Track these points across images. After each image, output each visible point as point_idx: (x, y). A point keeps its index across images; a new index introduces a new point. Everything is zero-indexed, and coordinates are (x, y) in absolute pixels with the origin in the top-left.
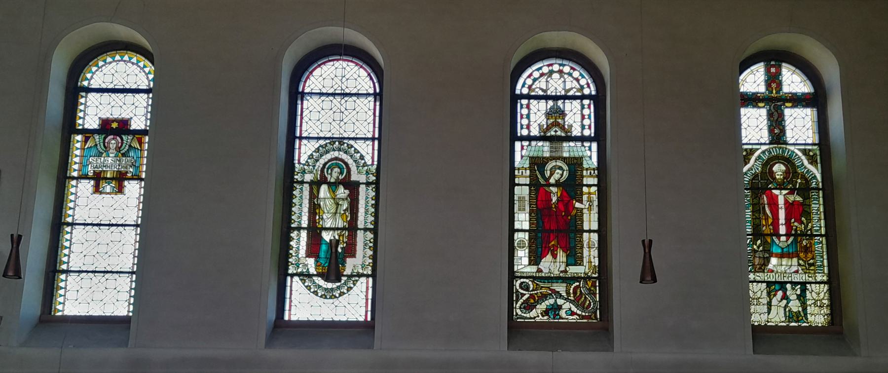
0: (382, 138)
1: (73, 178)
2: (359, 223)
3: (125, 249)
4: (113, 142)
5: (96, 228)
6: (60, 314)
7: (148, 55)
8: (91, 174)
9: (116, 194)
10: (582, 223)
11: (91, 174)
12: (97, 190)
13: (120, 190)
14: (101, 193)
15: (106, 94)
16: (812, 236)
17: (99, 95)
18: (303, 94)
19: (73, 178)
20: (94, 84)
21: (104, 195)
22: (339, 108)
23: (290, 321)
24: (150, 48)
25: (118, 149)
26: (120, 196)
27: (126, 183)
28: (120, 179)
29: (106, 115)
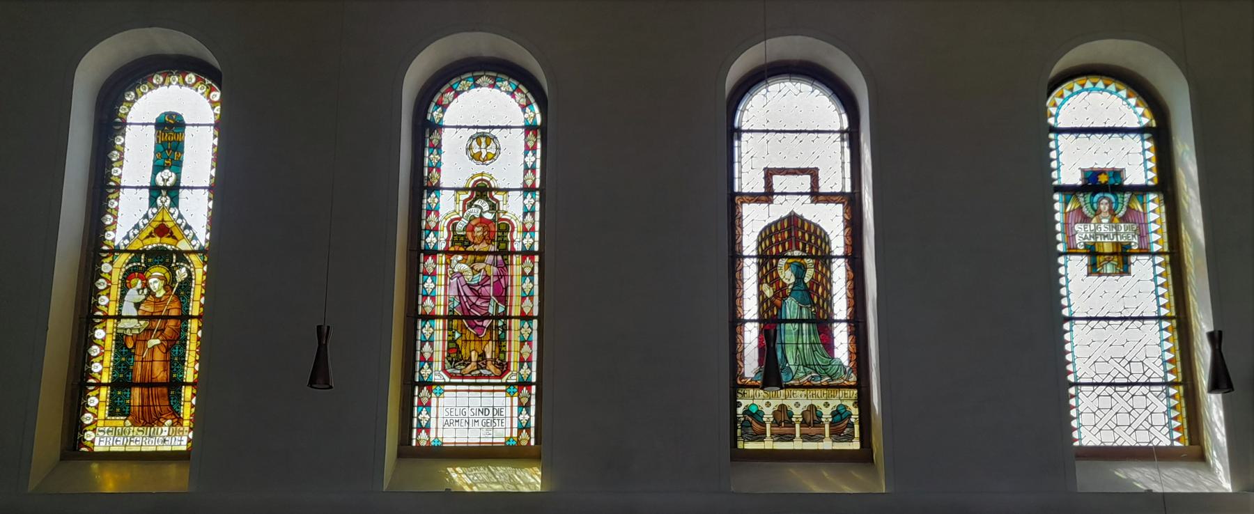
0: (552, 189)
1: (1061, 254)
2: (836, 310)
3: (1085, 351)
4: (1105, 201)
5: (1104, 323)
6: (1076, 444)
7: (204, 71)
8: (1081, 247)
9: (1121, 274)
10: (830, 304)
11: (1081, 247)
12: (1093, 269)
13: (1124, 270)
14: (1100, 274)
15: (1115, 135)
16: (510, 318)
17: (1073, 136)
18: (739, 131)
19: (1061, 254)
20: (1062, 124)
21: (1103, 278)
22: (485, 143)
23: (418, 446)
24: (215, 62)
25: (1112, 212)
26: (1125, 278)
27: (1133, 259)
28: (1123, 255)
29: (1089, 165)
